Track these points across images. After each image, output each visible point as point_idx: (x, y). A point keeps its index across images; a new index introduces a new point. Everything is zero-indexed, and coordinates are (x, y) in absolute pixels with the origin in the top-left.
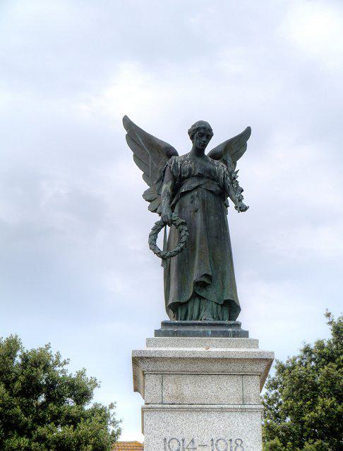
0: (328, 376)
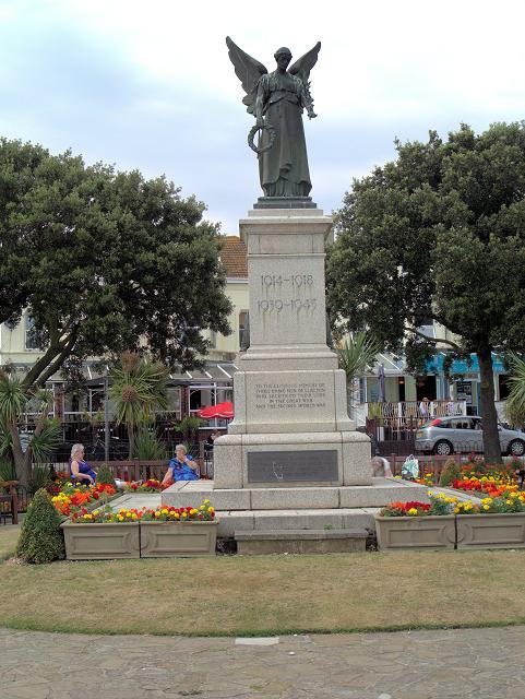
0: (392, 196)
